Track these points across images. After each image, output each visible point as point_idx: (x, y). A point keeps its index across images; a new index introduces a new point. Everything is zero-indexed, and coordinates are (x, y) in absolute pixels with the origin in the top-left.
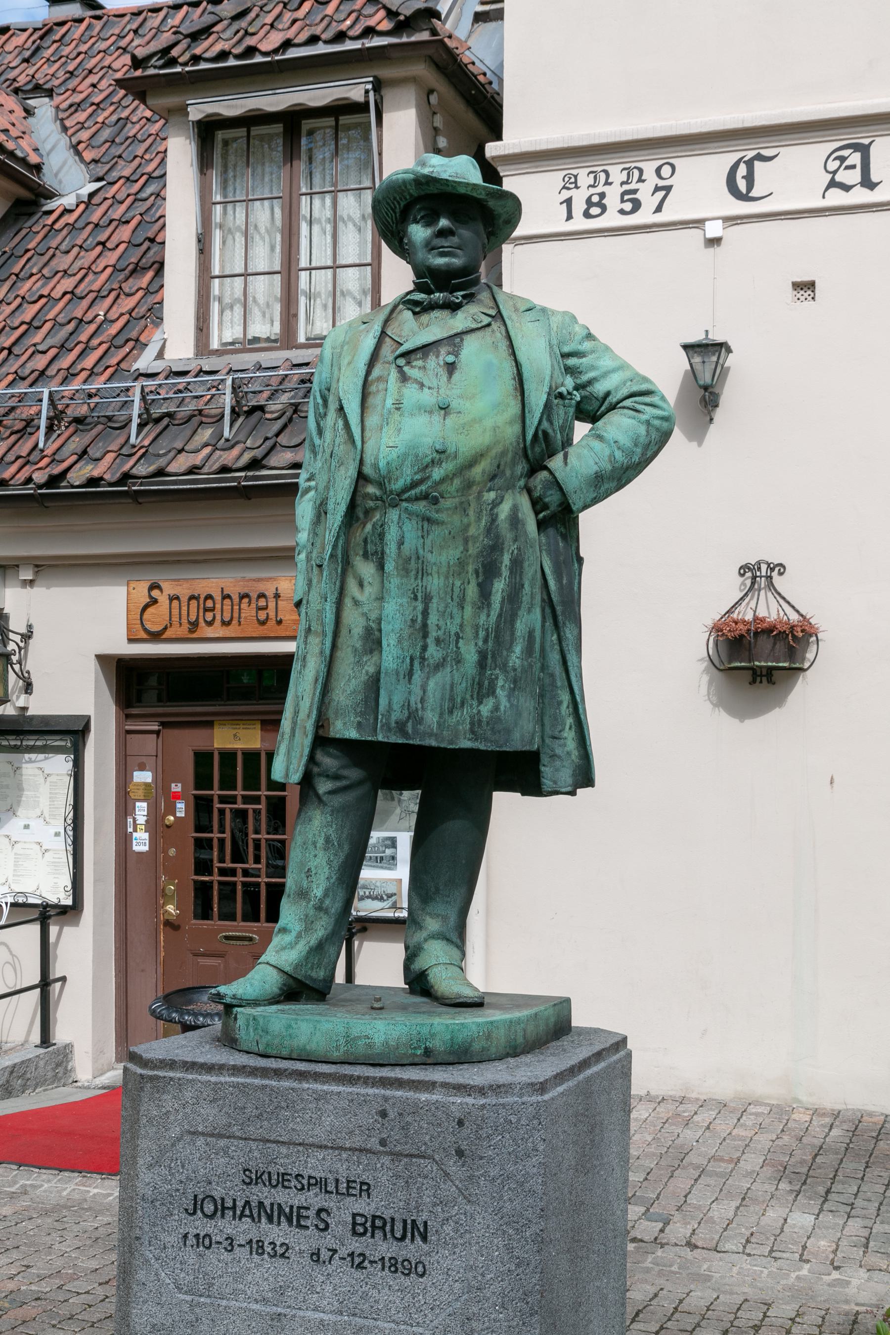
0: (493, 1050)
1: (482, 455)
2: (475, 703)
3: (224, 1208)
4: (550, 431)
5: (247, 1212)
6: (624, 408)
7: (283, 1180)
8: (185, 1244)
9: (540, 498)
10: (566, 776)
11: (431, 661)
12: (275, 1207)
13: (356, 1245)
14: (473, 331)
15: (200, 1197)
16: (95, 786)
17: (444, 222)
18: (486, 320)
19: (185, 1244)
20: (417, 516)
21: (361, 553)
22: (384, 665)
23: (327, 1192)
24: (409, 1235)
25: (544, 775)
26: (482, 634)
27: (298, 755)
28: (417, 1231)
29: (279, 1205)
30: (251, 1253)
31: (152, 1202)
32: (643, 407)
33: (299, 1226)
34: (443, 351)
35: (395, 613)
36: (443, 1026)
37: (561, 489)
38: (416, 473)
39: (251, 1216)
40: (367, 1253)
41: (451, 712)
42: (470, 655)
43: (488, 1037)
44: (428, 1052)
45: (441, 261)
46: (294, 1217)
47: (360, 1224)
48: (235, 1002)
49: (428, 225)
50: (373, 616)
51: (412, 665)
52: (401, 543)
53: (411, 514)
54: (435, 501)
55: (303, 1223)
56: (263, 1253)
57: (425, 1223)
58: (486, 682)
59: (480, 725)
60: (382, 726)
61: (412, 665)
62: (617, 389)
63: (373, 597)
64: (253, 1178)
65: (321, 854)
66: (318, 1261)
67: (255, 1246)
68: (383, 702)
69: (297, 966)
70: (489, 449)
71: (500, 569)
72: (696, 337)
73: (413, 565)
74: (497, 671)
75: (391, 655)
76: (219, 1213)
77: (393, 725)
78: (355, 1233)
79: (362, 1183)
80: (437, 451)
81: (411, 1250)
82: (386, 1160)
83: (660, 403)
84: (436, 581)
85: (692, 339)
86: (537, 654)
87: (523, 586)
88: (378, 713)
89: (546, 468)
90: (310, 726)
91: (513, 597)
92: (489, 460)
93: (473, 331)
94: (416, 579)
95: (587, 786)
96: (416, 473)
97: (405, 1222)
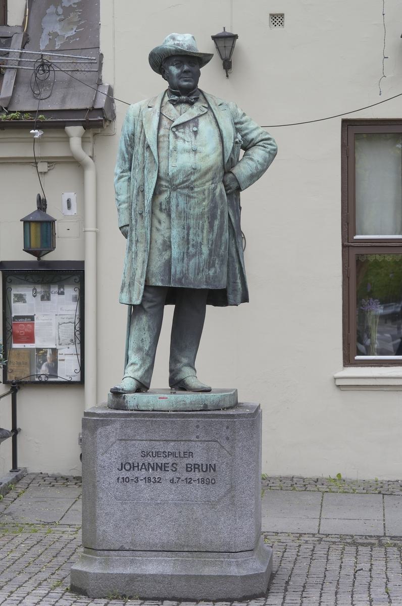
0: (118, 425)
1: (209, 170)
2: (207, 270)
3: (134, 467)
4: (233, 158)
5: (144, 467)
6: (259, 145)
7: (158, 454)
8: (118, 482)
9: (229, 185)
10: (239, 297)
11: (191, 254)
12: (155, 464)
13: (186, 475)
14: (201, 115)
15: (124, 464)
16: (343, 337)
17: (186, 68)
18: (206, 110)
19: (118, 482)
20: (184, 195)
21: (159, 209)
22: (173, 256)
23: (176, 457)
24: (209, 470)
25: (230, 298)
26: (210, 243)
27: (137, 293)
28: (211, 468)
29: (157, 463)
30: (146, 482)
31: (104, 467)
32: (267, 145)
33: (165, 470)
34: (191, 125)
35: (176, 234)
36: (187, 398)
37: (238, 181)
38: (184, 178)
39: (145, 469)
40: (193, 478)
41: (198, 274)
42: (205, 250)
43: (224, 400)
44: (206, 406)
45: (185, 84)
46: (163, 467)
47: (189, 468)
48: (123, 392)
49: (178, 68)
50: (167, 235)
51: (183, 256)
52: (177, 206)
53: (181, 194)
54: (192, 189)
55: (166, 469)
56: (151, 482)
57: (215, 465)
58: (212, 262)
59: (209, 279)
60: (173, 281)
61: (183, 256)
62: (256, 137)
63: (166, 228)
64: (145, 454)
65: (147, 333)
66: (173, 482)
67: (147, 479)
68: (173, 270)
69: (141, 378)
70: (212, 167)
71: (217, 216)
72: (218, 31)
73: (183, 215)
74: (216, 257)
75: (176, 251)
76: (132, 469)
77: (177, 280)
78: (187, 471)
79: (189, 453)
80: (193, 169)
81: (210, 475)
82: (199, 444)
83: (273, 143)
84: (192, 221)
85: (215, 34)
86: (228, 249)
87: (224, 222)
88: (170, 275)
89: (231, 172)
90: (143, 281)
91: (221, 227)
92: (212, 172)
93: (201, 115)
94: (184, 220)
95: (246, 302)
96: (184, 178)
97: (207, 465)
